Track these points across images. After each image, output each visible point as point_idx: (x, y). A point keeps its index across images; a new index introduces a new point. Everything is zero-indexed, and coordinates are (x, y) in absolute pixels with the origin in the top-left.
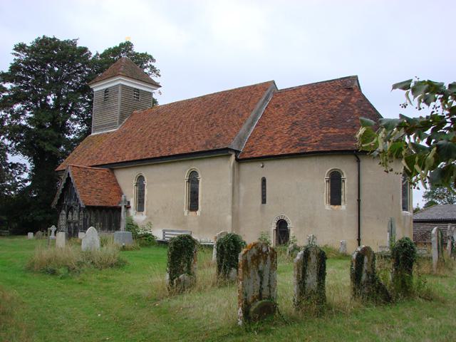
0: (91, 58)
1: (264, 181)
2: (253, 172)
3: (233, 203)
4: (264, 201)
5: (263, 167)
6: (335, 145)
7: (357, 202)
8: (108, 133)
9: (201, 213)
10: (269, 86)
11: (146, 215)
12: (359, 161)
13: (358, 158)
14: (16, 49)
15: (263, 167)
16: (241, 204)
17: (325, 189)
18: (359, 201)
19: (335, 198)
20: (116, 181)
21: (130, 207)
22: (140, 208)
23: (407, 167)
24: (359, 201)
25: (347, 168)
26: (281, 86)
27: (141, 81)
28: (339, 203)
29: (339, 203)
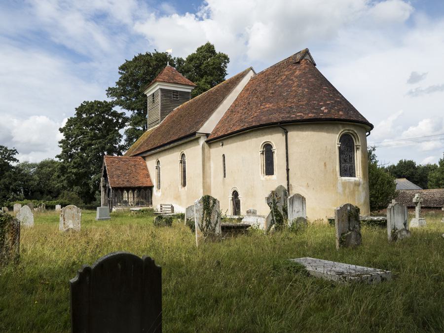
0: (439, 166)
2: (217, 151)
3: (204, 178)
4: (225, 177)
5: (222, 145)
6: (264, 120)
7: (286, 171)
12: (286, 133)
13: (285, 130)
14: (120, 69)
15: (222, 145)
16: (212, 179)
17: (260, 160)
18: (288, 170)
20: (146, 166)
21: (88, 200)
22: (159, 187)
23: (355, 141)
24: (288, 170)
25: (276, 139)
27: (178, 84)
28: (272, 174)
29: (272, 174)
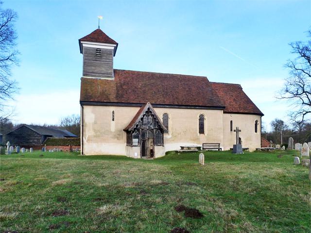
1: (202, 119)
7: (84, 125)
8: (107, 80)
9: (208, 135)
10: (204, 79)
11: (172, 135)
19: (256, 131)
26: (211, 80)
